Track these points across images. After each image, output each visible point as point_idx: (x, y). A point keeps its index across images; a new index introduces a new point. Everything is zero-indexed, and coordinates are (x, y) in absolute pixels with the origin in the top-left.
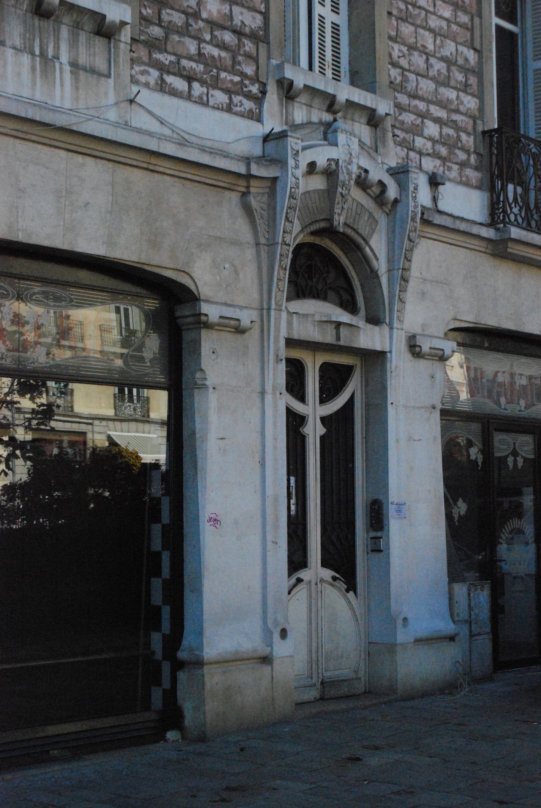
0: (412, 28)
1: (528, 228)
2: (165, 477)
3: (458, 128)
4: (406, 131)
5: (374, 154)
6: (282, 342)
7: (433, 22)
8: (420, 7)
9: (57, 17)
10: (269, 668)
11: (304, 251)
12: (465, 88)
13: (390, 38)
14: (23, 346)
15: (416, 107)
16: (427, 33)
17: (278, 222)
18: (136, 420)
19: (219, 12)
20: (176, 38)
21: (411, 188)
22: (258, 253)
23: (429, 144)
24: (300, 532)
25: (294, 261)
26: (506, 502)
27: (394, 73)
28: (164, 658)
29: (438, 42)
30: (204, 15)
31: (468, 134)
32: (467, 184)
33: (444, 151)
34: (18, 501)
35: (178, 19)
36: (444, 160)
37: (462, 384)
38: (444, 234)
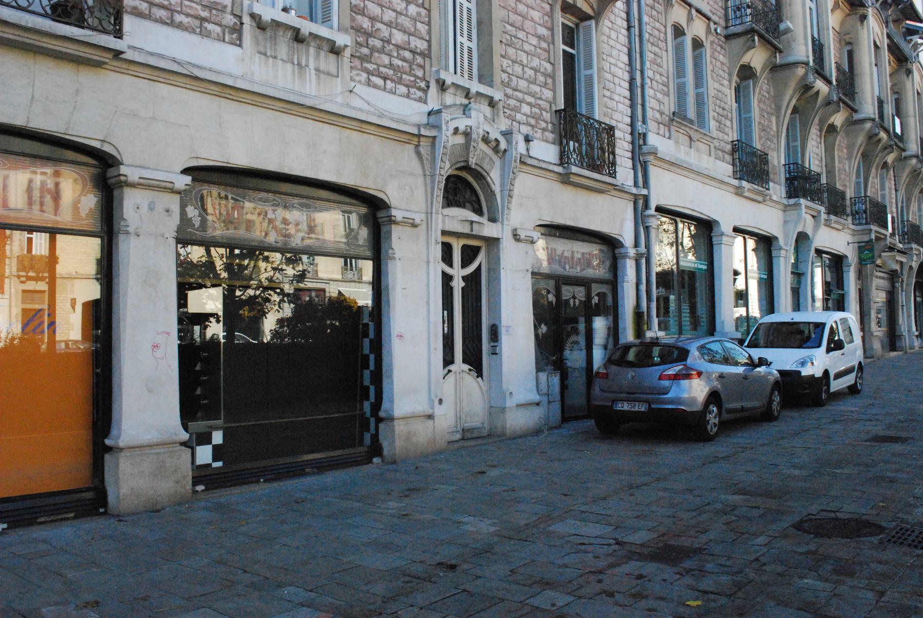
0: (514, 50)
1: (582, 167)
2: (371, 314)
3: (541, 109)
4: (512, 110)
5: (492, 123)
6: (439, 233)
7: (527, 47)
8: (518, 38)
9: (308, 42)
10: (432, 421)
11: (452, 179)
12: (545, 85)
13: (502, 56)
14: (287, 236)
15: (517, 96)
16: (523, 53)
17: (437, 161)
18: (354, 281)
19: (402, 40)
20: (376, 54)
21: (514, 143)
22: (425, 179)
23: (524, 118)
24: (450, 343)
25: (446, 185)
26: (569, 327)
27: (504, 76)
28: (372, 416)
29: (529, 58)
30: (393, 42)
31: (547, 112)
32: (546, 141)
33: (533, 122)
34: (286, 328)
35: (378, 44)
36: (533, 127)
37: (544, 260)
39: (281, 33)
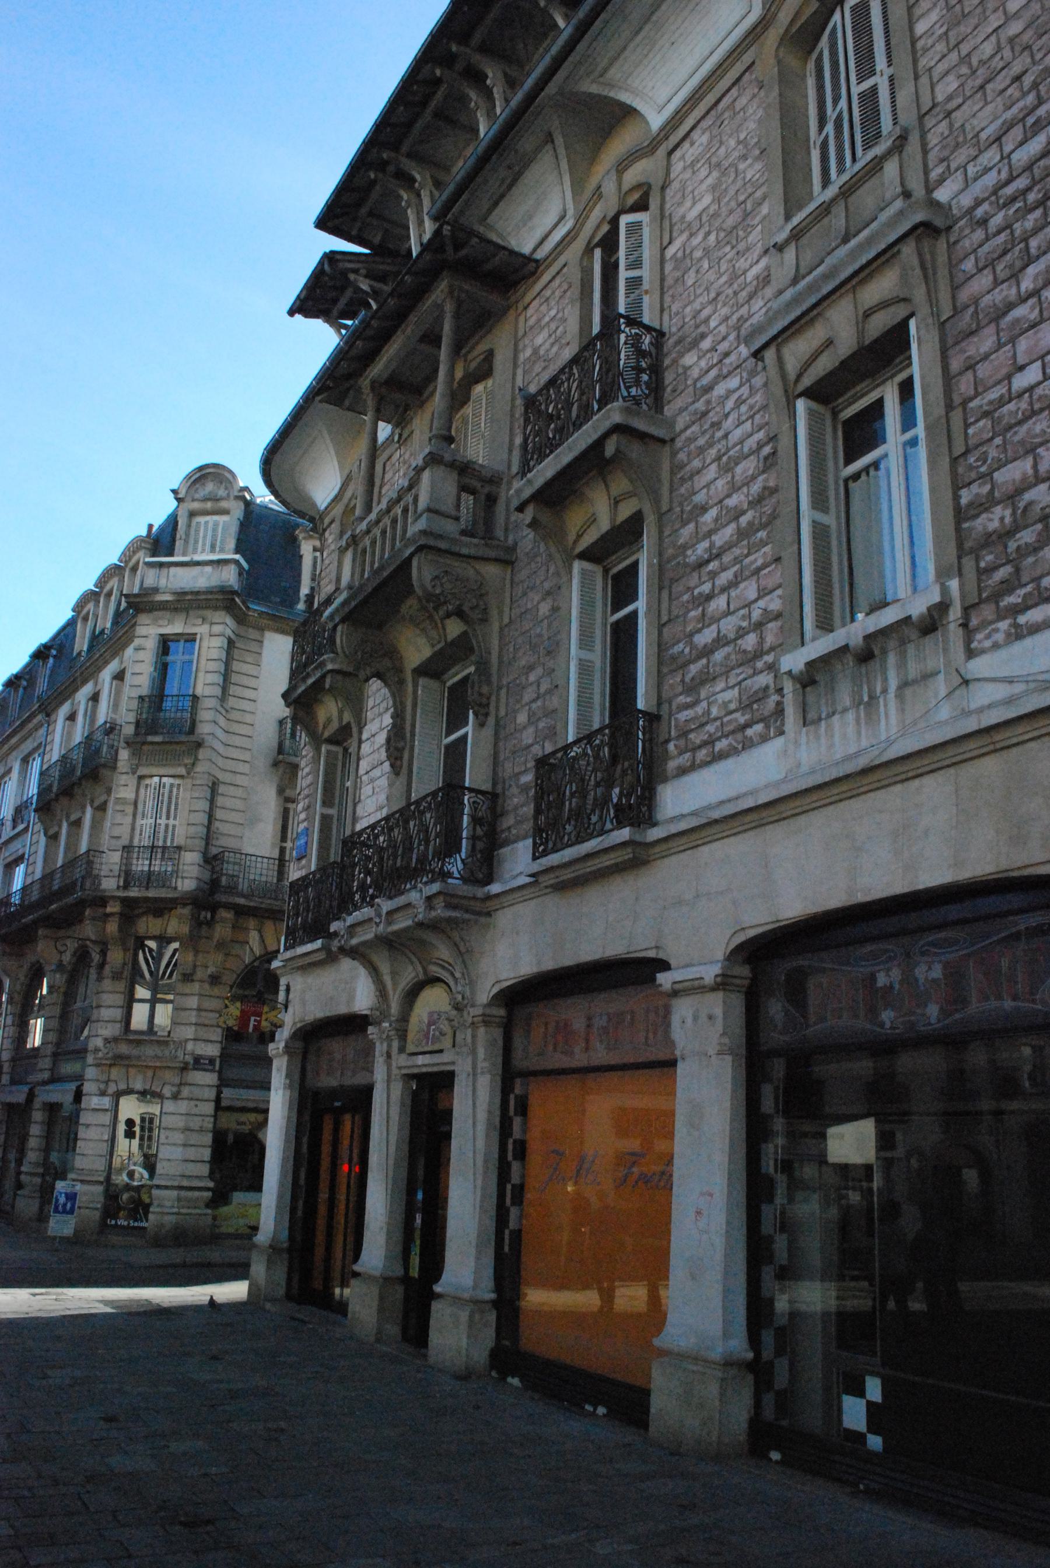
38: (918, 763)
39: (839, 667)
